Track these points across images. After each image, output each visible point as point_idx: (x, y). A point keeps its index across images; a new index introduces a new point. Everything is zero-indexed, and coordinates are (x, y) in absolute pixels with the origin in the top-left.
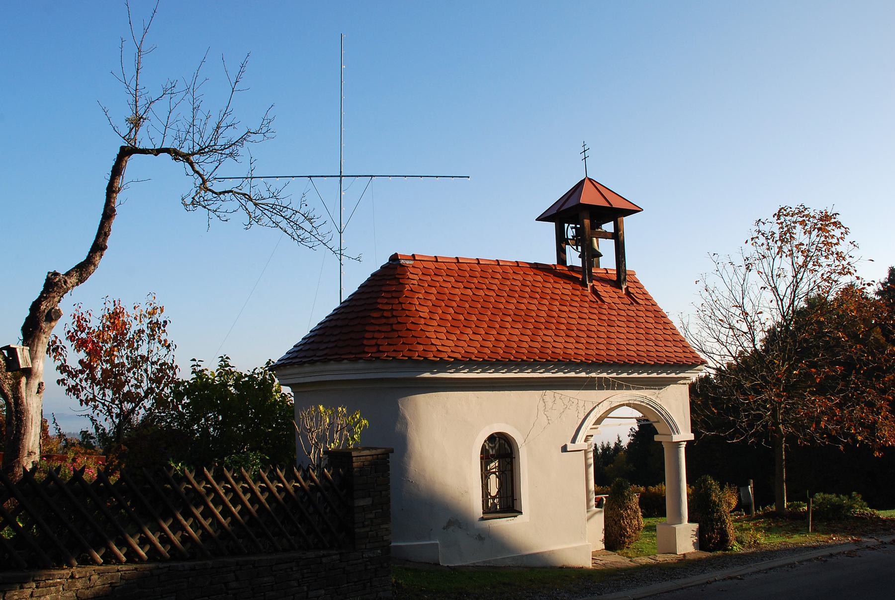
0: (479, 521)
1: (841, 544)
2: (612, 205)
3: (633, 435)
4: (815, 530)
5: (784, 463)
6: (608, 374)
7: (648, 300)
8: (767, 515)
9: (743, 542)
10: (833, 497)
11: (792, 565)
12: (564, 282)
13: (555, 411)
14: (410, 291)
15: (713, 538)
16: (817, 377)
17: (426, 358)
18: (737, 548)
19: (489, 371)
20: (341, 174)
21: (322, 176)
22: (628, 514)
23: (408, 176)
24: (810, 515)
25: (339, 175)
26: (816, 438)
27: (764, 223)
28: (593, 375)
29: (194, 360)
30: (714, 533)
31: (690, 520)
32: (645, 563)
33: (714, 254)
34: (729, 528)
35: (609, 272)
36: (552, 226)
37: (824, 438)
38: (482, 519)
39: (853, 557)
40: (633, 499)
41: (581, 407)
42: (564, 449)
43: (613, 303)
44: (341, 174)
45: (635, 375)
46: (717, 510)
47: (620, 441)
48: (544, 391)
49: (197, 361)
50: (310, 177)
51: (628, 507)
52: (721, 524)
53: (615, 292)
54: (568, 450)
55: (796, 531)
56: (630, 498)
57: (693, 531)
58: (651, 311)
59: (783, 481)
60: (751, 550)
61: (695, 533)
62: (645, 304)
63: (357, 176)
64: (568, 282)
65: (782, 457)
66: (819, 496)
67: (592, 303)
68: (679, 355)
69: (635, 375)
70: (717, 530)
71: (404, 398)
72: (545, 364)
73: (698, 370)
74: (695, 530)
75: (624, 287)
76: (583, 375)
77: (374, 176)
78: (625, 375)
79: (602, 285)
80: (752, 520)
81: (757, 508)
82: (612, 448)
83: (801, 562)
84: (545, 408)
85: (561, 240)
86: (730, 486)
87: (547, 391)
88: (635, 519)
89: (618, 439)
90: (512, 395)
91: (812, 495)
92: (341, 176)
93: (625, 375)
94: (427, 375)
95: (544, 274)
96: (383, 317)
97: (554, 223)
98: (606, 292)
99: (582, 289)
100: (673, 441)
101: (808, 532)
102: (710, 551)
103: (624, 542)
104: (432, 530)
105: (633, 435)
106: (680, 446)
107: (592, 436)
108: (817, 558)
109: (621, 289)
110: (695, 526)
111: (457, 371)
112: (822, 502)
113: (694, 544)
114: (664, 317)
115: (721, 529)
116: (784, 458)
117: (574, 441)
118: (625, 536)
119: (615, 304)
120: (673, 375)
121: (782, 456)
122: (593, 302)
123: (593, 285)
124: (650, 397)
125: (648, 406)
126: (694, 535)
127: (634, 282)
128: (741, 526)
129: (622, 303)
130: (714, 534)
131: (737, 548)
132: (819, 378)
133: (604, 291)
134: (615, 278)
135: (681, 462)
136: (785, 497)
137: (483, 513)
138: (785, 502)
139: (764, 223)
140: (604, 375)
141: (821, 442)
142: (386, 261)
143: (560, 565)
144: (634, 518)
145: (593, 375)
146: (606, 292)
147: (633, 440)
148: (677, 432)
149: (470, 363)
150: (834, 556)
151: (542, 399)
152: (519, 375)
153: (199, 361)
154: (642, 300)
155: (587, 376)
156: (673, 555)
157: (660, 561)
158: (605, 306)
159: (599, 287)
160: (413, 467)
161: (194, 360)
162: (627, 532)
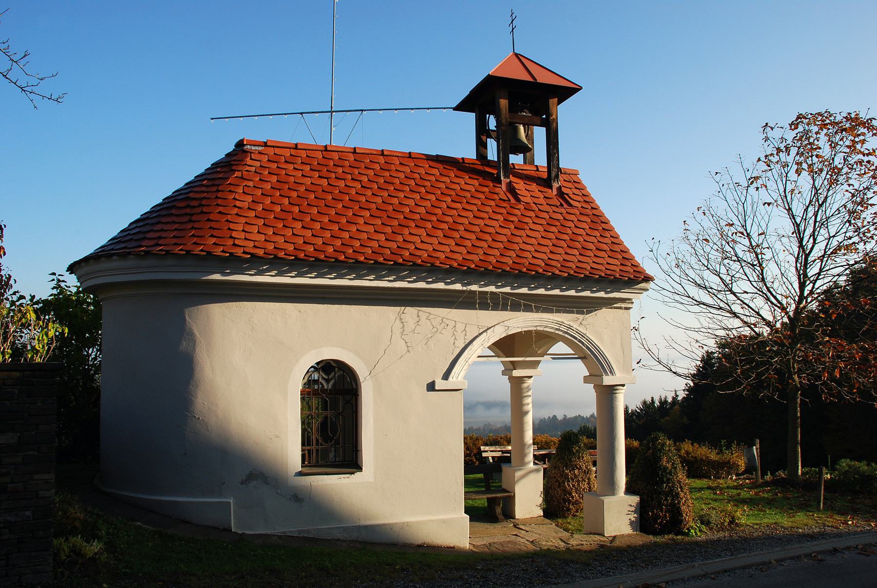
0: (295, 476)
1: (856, 533)
2: (536, 80)
3: (687, 390)
4: (830, 508)
5: (799, 420)
6: (497, 287)
7: (588, 202)
8: (775, 483)
9: (711, 523)
10: (863, 466)
11: (764, 566)
12: (470, 177)
13: (419, 335)
14: (240, 178)
15: (659, 517)
16: (833, 312)
17: (210, 252)
18: (697, 533)
19: (329, 276)
20: (332, 109)
21: (313, 113)
22: (575, 475)
23: (398, 109)
24: (823, 487)
25: (330, 110)
26: (844, 393)
27: (772, 128)
28: (474, 288)
29: (54, 274)
30: (662, 510)
31: (629, 490)
32: (546, 548)
33: (717, 173)
34: (684, 504)
35: (540, 170)
36: (470, 118)
37: (853, 394)
38: (300, 474)
39: (867, 556)
40: (583, 457)
41: (459, 332)
42: (431, 387)
43: (534, 203)
44: (332, 109)
45: (541, 291)
46: (668, 479)
47: (677, 396)
48: (403, 308)
49: (57, 275)
50: (301, 113)
51: (576, 466)
52: (673, 499)
53: (541, 192)
54: (437, 388)
55: (804, 506)
56: (579, 455)
57: (631, 505)
58: (588, 215)
59: (797, 443)
60: (721, 534)
61: (633, 509)
62: (582, 207)
63: (348, 111)
64: (475, 177)
65: (797, 414)
66: (844, 463)
67: (503, 201)
68: (605, 264)
69: (541, 291)
70: (666, 506)
71: (193, 308)
72: (396, 268)
73: (640, 289)
74: (635, 505)
75: (555, 185)
76: (458, 287)
77: (365, 110)
78: (524, 290)
79: (524, 183)
80: (755, 488)
81: (764, 474)
82: (669, 401)
83: (780, 561)
84: (404, 331)
85: (482, 131)
86: (738, 444)
87: (407, 308)
88: (585, 481)
89: (676, 393)
90: (353, 310)
91: (835, 462)
92: (331, 112)
93: (524, 290)
94: (217, 277)
95: (444, 168)
96: (188, 206)
97: (474, 114)
98: (528, 191)
99: (494, 186)
100: (604, 384)
101: (818, 510)
102: (655, 533)
103: (569, 509)
104: (224, 483)
105: (687, 390)
106: (615, 392)
107: (531, 377)
108: (809, 556)
109: (551, 187)
110: (635, 499)
111: (260, 273)
112: (847, 471)
113: (632, 523)
114: (606, 222)
115: (673, 505)
116: (799, 415)
117: (446, 377)
118: (569, 502)
119: (536, 204)
120: (602, 294)
121: (797, 412)
122: (504, 200)
123: (510, 181)
124: (568, 323)
125: (566, 336)
126: (632, 511)
127: (574, 182)
128: (739, 494)
129: (547, 204)
130: (662, 510)
131: (697, 533)
132: (835, 313)
133: (526, 189)
134: (545, 176)
135: (616, 413)
136: (800, 463)
137: (302, 467)
138: (800, 468)
139: (772, 128)
140: (492, 289)
141: (851, 398)
142: (231, 148)
143: (420, 542)
144: (584, 480)
145: (474, 288)
146: (528, 191)
147: (687, 395)
148: (611, 372)
149: (277, 263)
150: (839, 551)
151: (398, 318)
152: (356, 282)
153: (59, 275)
154: (579, 202)
155: (465, 288)
156: (597, 538)
157: (573, 546)
158: (521, 207)
159: (520, 186)
160: (201, 401)
161: (54, 274)
162: (573, 497)
